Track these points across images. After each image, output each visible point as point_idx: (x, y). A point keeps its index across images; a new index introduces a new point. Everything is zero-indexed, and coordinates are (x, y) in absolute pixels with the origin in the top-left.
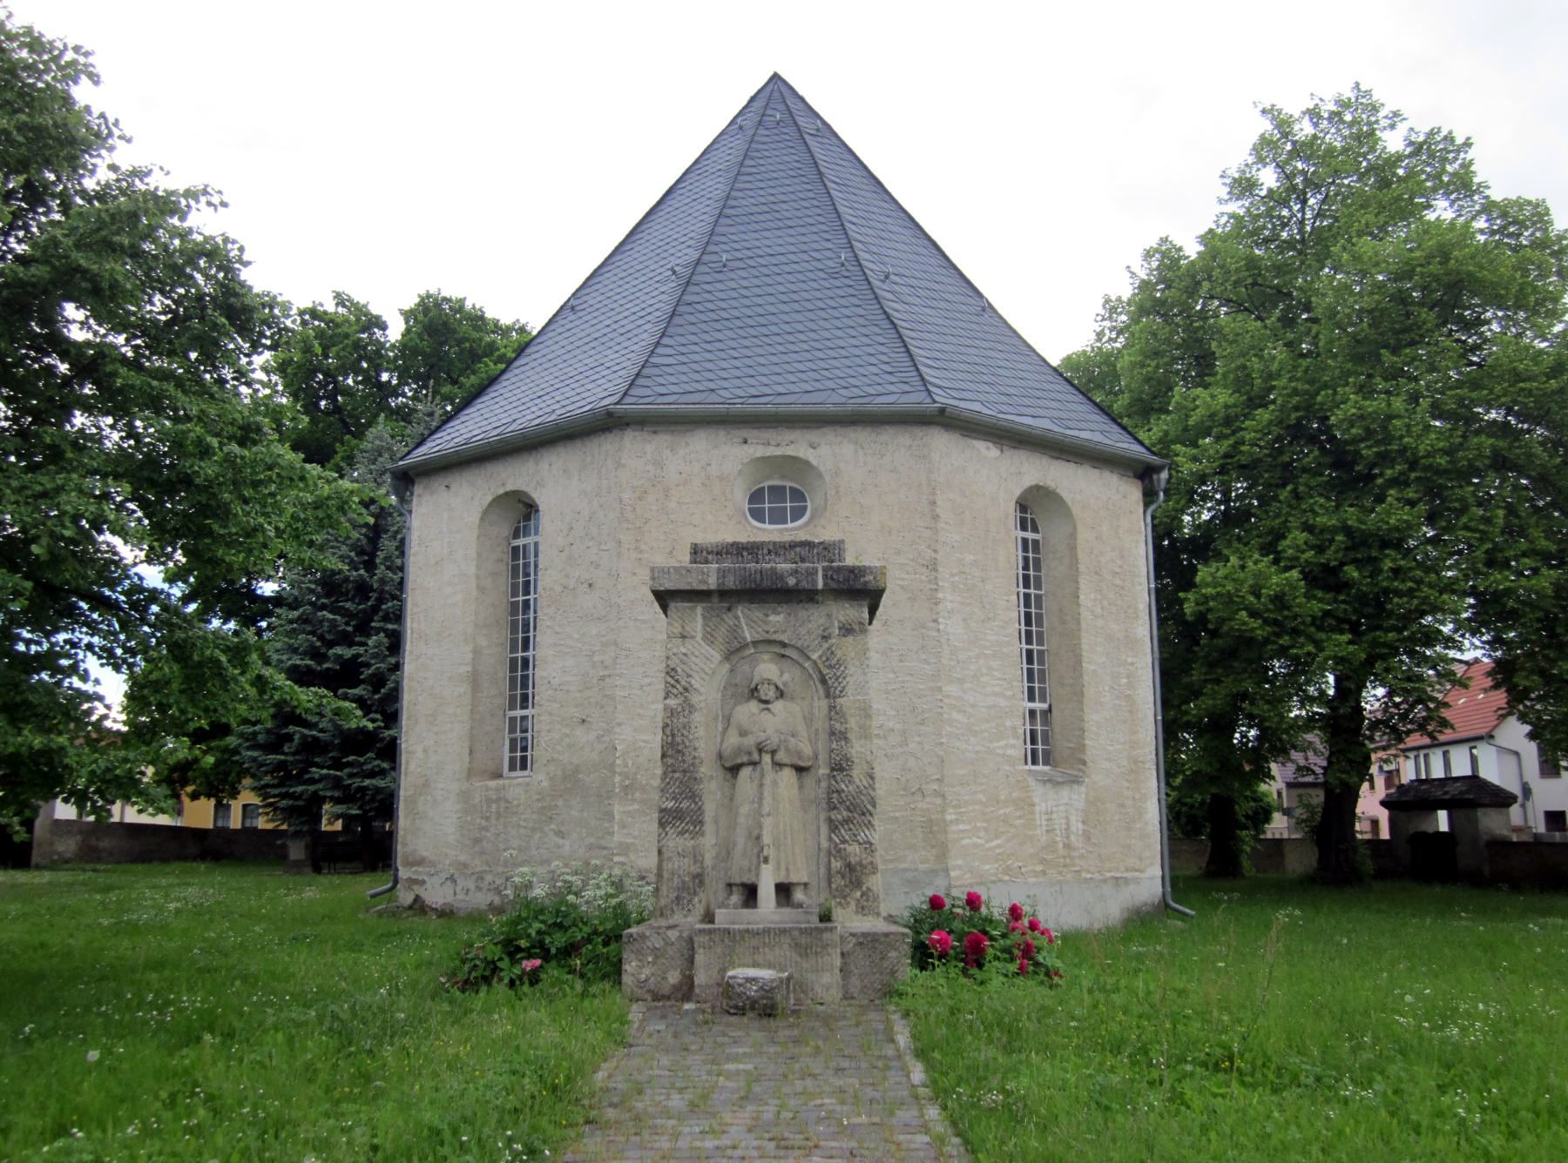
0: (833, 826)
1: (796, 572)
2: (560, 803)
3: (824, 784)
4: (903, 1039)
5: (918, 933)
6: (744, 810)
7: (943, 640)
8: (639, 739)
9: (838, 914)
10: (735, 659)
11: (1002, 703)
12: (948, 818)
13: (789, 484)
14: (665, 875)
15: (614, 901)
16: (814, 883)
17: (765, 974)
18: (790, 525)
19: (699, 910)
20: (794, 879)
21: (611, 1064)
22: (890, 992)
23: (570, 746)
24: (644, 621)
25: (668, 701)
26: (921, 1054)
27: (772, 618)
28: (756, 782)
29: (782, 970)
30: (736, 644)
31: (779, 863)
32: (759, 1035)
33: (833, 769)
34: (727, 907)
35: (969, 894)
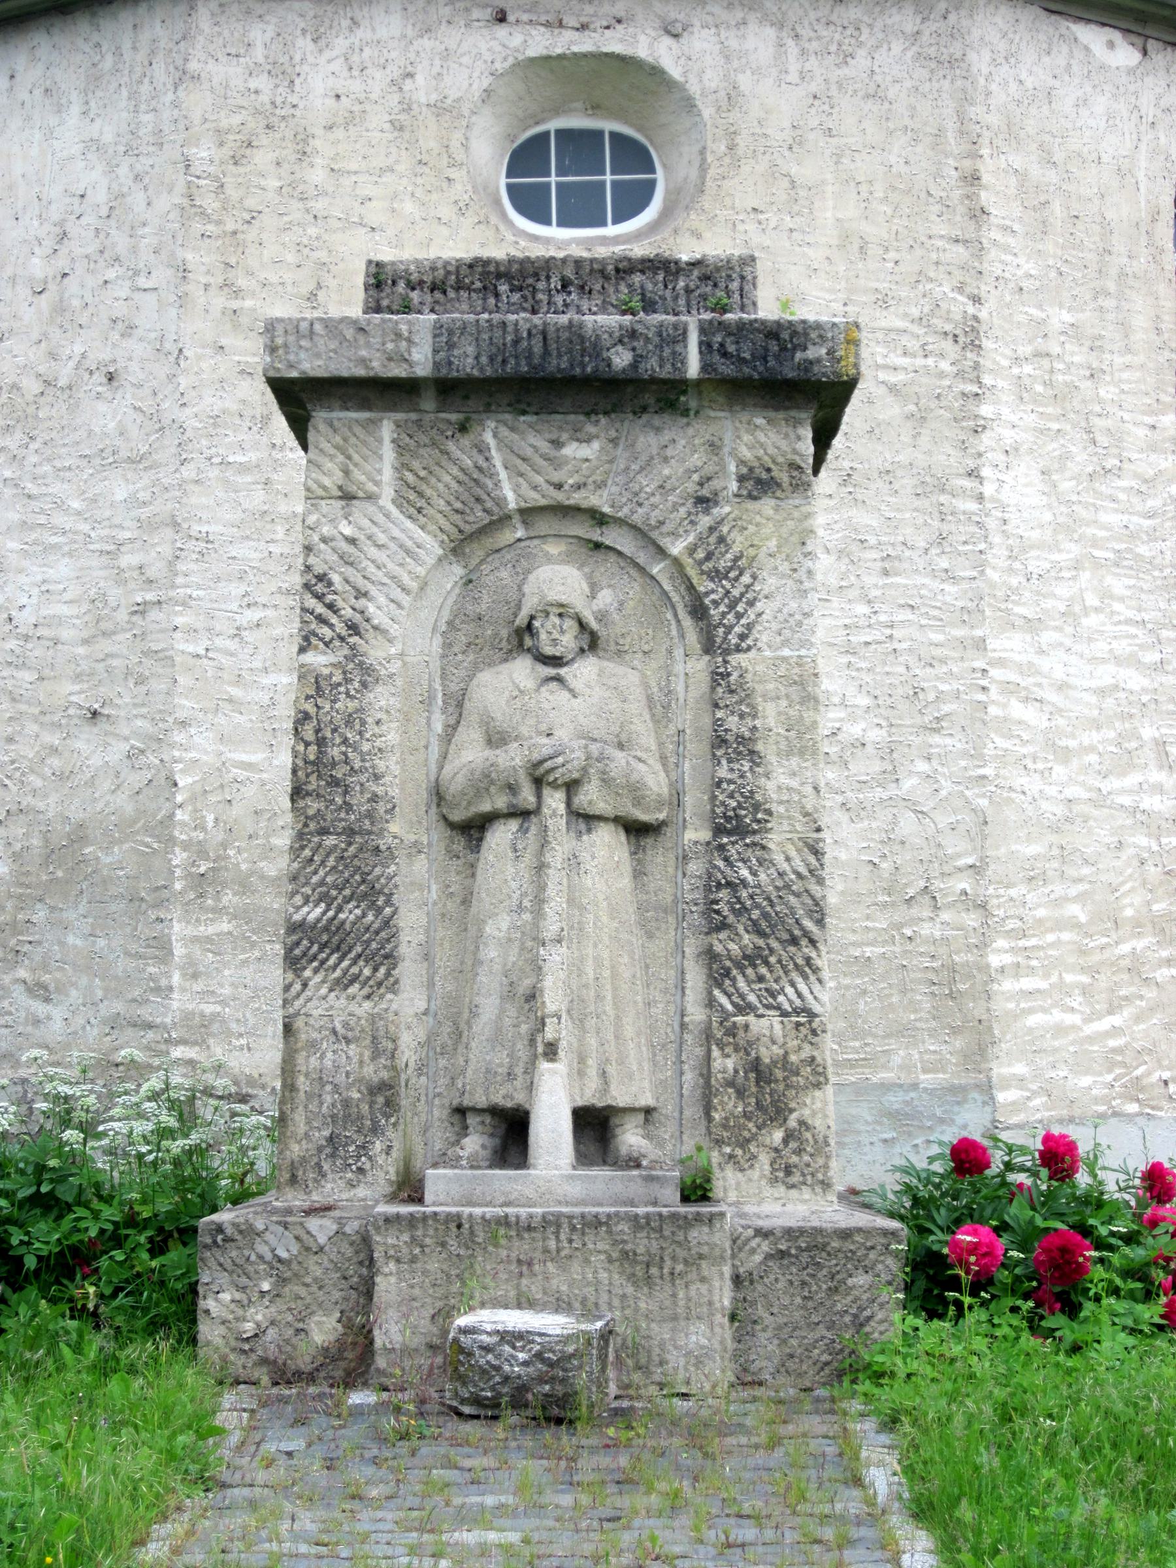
0: (718, 972)
1: (633, 334)
2: (40, 915)
3: (696, 867)
4: (883, 1477)
5: (923, 1231)
6: (498, 926)
7: (992, 524)
8: (232, 755)
9: (728, 1184)
10: (476, 552)
11: (1135, 680)
12: (995, 960)
13: (609, 126)
14: (302, 1082)
15: (177, 1146)
16: (669, 1109)
17: (552, 1324)
18: (611, 230)
19: (385, 1170)
20: (620, 1097)
21: (174, 1528)
22: (850, 1369)
23: (61, 777)
24: (244, 468)
25: (310, 658)
26: (924, 1511)
27: (571, 450)
28: (528, 859)
29: (589, 1314)
30: (480, 517)
31: (582, 1060)
32: (535, 1467)
33: (718, 831)
34: (455, 1163)
35: (1048, 1138)
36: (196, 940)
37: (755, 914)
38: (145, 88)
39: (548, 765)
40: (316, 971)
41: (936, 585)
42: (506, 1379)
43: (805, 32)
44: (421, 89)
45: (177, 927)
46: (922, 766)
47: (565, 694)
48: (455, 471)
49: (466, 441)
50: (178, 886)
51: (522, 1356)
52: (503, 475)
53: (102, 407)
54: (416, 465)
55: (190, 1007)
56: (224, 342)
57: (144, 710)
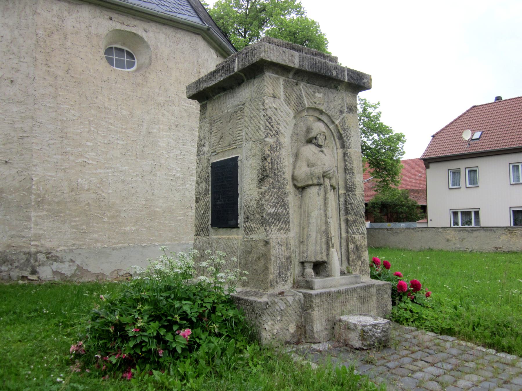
24: (50, 107)
27: (317, 94)
36: (37, 216)
37: (355, 211)
38: (23, 14)
39: (329, 172)
40: (274, 226)
41: (192, 148)
42: (376, 338)
43: (170, 37)
44: (93, 30)
45: (33, 213)
46: (190, 183)
47: (323, 155)
48: (296, 95)
49: (297, 87)
50: (33, 204)
51: (379, 331)
52: (305, 98)
53: (9, 88)
54: (288, 91)
55: (36, 232)
56: (46, 77)
57: (23, 162)
